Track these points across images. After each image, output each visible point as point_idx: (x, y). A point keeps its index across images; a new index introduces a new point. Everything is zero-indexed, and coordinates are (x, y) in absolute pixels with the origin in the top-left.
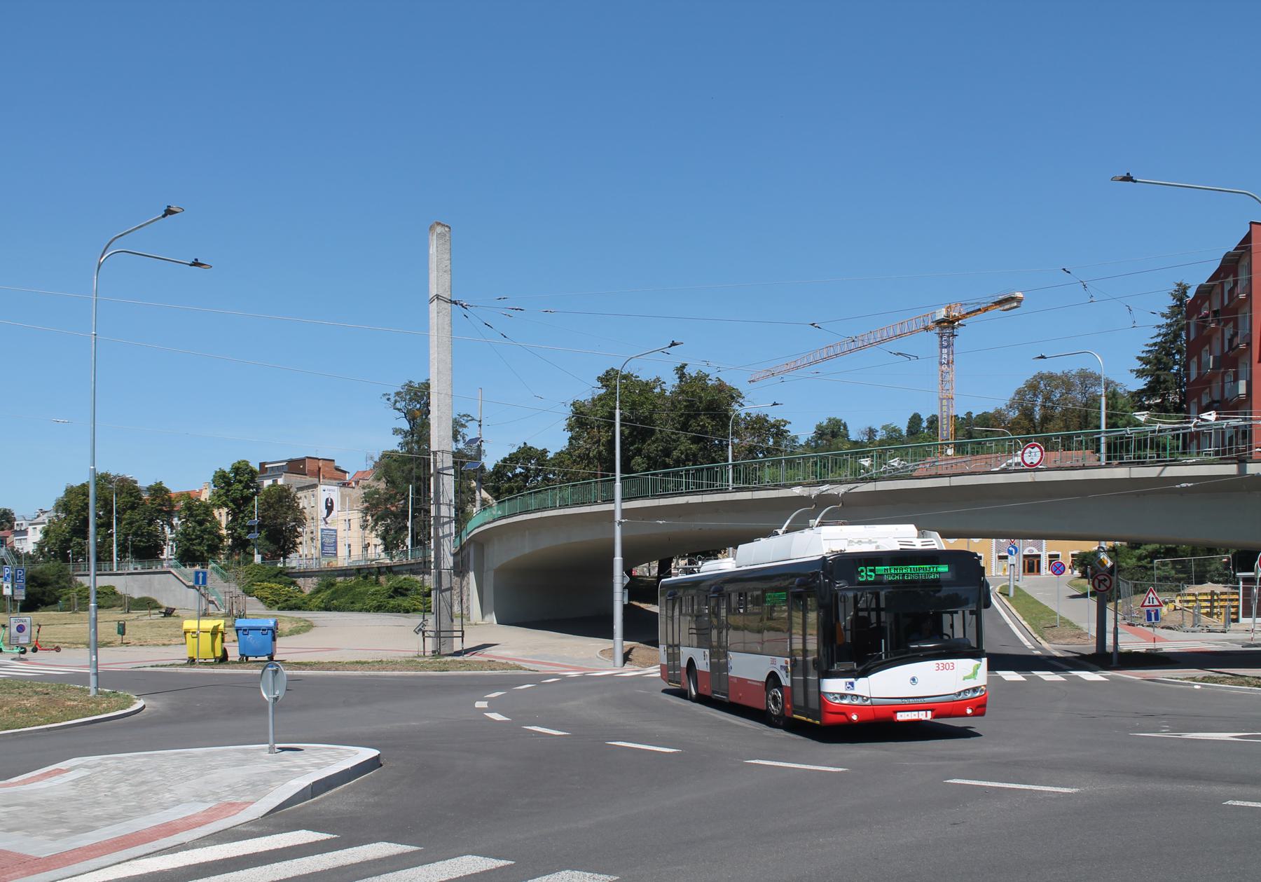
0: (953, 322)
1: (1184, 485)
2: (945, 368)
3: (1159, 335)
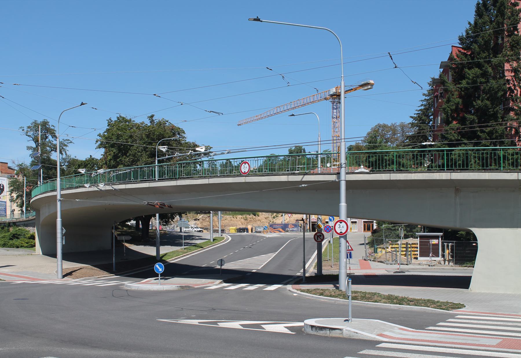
1: (303, 185)
2: (335, 120)
3: (422, 105)
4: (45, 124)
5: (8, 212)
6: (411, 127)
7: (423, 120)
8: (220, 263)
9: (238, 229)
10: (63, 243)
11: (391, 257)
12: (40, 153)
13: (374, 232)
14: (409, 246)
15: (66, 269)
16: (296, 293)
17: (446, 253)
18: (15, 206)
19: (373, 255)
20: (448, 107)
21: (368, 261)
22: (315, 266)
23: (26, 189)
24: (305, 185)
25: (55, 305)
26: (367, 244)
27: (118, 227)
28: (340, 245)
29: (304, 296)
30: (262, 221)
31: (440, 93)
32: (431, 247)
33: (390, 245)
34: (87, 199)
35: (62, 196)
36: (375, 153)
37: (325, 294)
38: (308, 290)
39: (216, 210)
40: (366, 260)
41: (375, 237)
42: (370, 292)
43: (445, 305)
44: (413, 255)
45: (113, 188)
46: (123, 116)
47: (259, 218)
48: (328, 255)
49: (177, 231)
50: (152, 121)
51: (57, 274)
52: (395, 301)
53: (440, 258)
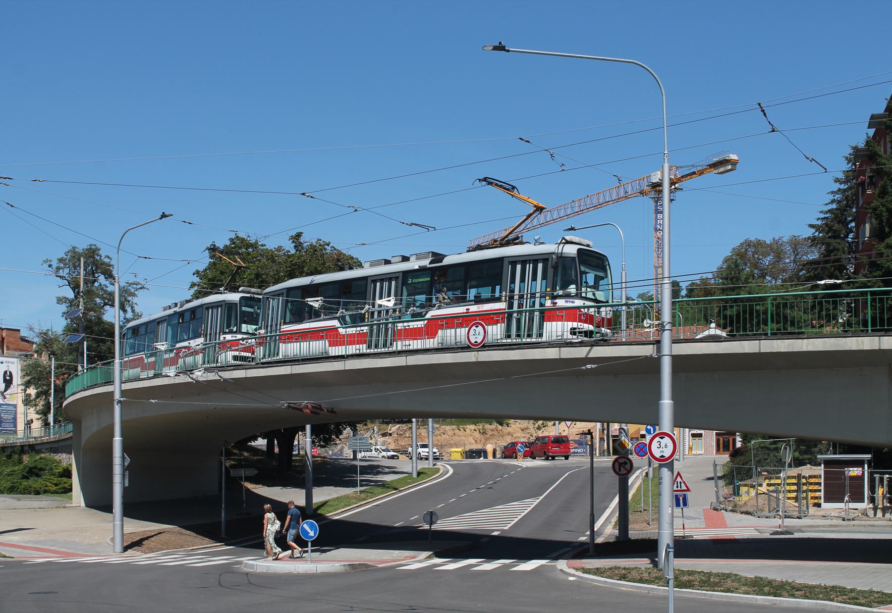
1: (589, 366)
3: (833, 201)
4: (92, 253)
5: (21, 426)
6: (811, 246)
7: (835, 231)
8: (428, 518)
9: (466, 452)
10: (124, 484)
11: (766, 502)
12: (82, 311)
13: (736, 454)
14: (804, 481)
15: (130, 533)
16: (574, 575)
17: (878, 494)
18: (32, 414)
19: (731, 499)
20: (883, 205)
21: (722, 511)
22: (616, 523)
23: (54, 381)
24: (593, 366)
25: (108, 604)
26: (720, 478)
27: (233, 451)
28: (661, 481)
29: (588, 582)
30: (515, 435)
31: (869, 177)
32: (847, 482)
33: (765, 480)
34: (172, 398)
35: (123, 393)
36: (736, 300)
37: (630, 577)
38: (597, 569)
39: (423, 417)
40: (717, 510)
41: (738, 464)
42: (719, 573)
43: (866, 596)
44: (812, 498)
45: (220, 377)
46: (242, 235)
47: (509, 429)
48: (642, 501)
49: (348, 458)
50: (298, 246)
51: (112, 544)
52: (766, 589)
53: (865, 505)
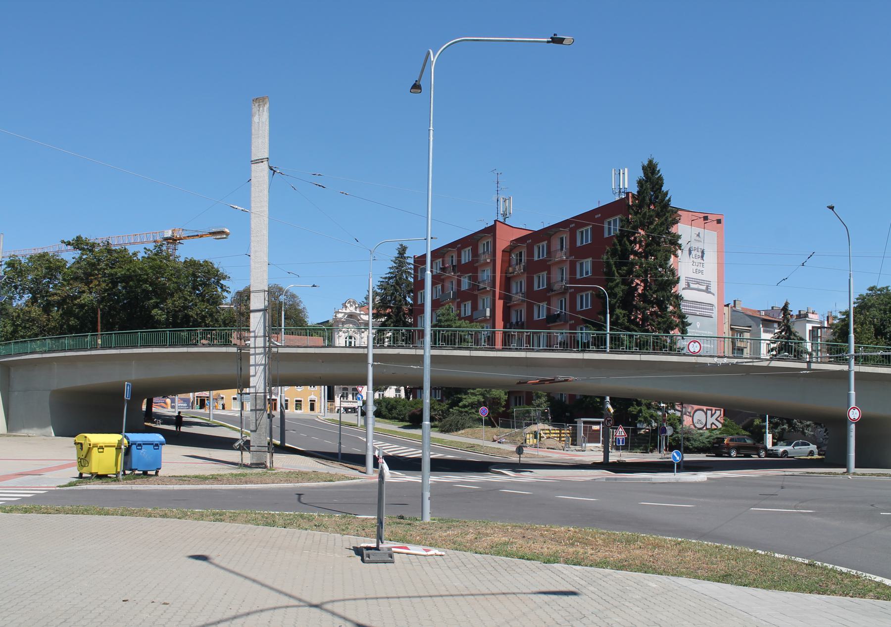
0: (176, 240)
3: (390, 273)
